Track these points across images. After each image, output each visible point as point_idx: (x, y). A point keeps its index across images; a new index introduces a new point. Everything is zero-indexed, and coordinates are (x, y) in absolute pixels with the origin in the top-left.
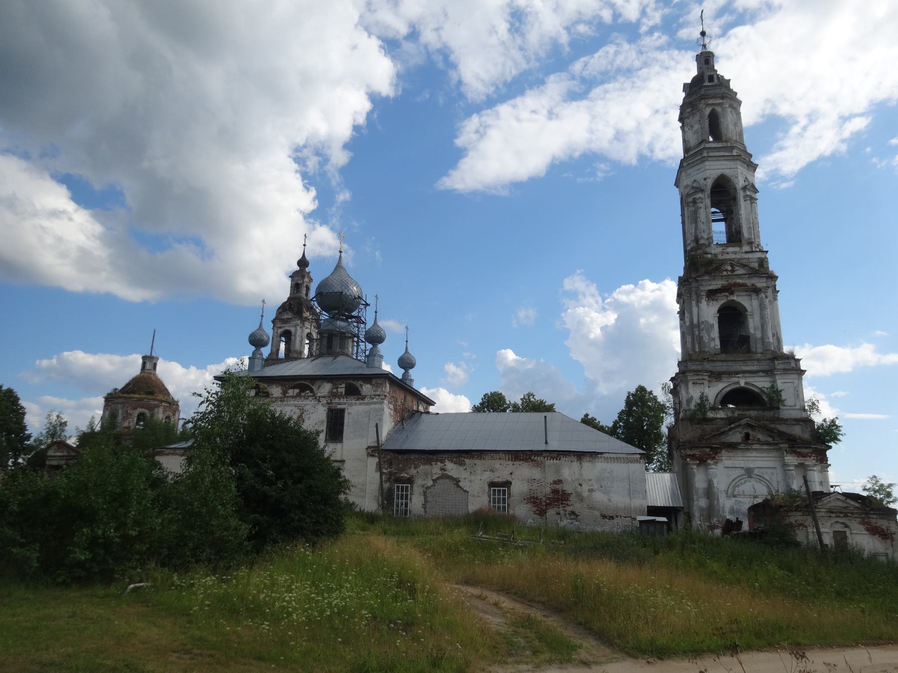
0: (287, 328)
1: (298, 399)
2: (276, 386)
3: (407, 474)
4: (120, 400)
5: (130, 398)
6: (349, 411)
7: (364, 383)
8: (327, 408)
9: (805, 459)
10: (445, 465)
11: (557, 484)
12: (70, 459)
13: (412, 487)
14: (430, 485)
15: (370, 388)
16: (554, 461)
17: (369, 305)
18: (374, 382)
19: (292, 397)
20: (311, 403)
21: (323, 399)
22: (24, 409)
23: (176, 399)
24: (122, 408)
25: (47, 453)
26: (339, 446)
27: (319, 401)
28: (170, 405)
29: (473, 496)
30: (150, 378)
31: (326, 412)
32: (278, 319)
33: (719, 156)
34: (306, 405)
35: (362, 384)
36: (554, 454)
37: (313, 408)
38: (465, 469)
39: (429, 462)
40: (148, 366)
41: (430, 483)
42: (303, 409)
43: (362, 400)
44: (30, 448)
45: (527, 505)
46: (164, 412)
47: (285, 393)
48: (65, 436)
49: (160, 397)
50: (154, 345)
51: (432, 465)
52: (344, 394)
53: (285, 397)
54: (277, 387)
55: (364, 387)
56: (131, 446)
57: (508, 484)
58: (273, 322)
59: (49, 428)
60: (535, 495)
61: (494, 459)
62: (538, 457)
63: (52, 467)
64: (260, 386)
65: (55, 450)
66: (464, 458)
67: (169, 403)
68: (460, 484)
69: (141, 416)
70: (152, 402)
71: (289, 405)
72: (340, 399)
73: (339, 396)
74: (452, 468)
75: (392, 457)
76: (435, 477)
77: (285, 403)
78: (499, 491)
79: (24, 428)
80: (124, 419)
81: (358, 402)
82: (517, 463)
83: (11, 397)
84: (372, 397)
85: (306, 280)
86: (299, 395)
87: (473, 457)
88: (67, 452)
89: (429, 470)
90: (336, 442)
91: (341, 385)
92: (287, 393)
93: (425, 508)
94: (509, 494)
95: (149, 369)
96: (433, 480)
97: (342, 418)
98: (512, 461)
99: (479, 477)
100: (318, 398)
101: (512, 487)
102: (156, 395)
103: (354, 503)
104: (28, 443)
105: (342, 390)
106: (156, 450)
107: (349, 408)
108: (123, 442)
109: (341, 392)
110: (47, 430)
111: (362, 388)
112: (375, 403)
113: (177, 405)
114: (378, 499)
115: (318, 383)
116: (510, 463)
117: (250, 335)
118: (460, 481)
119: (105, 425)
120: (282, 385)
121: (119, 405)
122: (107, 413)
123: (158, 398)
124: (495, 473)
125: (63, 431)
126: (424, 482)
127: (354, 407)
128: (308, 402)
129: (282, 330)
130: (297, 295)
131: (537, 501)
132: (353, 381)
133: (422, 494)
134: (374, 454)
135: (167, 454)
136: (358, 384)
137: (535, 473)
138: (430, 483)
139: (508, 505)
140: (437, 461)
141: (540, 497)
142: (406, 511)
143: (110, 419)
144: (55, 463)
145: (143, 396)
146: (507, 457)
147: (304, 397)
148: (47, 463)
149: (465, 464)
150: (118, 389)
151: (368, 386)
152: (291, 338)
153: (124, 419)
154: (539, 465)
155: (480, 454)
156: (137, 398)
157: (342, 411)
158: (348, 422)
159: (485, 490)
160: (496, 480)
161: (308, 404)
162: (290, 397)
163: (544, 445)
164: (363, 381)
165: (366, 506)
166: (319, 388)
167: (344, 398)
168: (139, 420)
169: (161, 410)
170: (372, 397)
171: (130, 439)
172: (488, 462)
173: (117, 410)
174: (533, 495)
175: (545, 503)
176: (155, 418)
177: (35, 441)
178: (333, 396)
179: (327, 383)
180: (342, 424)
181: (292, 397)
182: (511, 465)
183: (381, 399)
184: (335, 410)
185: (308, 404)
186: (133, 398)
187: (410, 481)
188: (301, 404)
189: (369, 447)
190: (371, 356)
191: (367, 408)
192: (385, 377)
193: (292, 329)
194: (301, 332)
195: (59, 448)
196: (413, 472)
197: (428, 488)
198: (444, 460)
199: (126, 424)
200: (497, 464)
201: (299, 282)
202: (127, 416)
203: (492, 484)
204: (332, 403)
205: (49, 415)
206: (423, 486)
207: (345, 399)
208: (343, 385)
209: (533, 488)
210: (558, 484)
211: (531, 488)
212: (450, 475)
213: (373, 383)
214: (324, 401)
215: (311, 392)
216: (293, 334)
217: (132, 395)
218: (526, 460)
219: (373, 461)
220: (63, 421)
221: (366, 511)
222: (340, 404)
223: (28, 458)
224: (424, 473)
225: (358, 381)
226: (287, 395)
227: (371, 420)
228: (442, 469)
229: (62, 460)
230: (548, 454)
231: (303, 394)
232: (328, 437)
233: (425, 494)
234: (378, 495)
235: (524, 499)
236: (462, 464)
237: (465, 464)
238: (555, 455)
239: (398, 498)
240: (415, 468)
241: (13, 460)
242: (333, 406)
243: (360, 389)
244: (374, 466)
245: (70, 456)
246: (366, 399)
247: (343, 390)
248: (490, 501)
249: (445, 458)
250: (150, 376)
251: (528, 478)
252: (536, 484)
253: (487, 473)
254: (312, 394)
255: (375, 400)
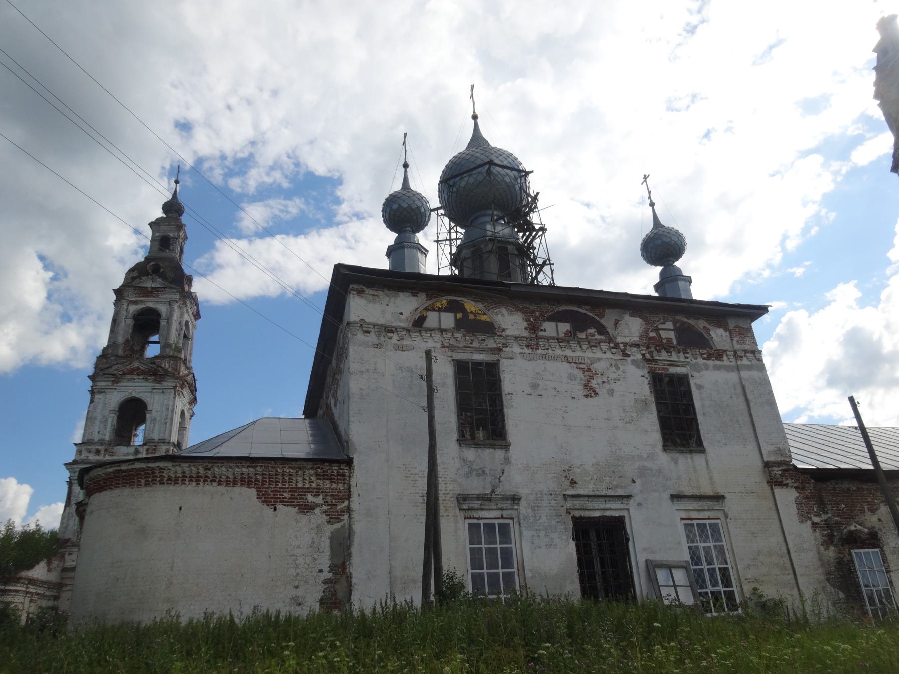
0: (151, 305)
3: (860, 525)
6: (698, 381)
9: (631, 538)
20: (604, 356)
21: (635, 349)
31: (646, 382)
32: (132, 286)
35: (708, 326)
37: (614, 369)
42: (589, 370)
43: (717, 359)
47: (533, 328)
58: (118, 292)
72: (668, 352)
73: (667, 347)
77: (540, 352)
81: (710, 363)
86: (569, 338)
91: (663, 323)
100: (621, 346)
117: (387, 200)
129: (139, 307)
151: (720, 331)
152: (159, 323)
158: (703, 406)
161: (599, 360)
185: (599, 360)
188: (583, 358)
193: (163, 309)
194: (179, 314)
215: (600, 333)
216: (164, 315)
221: (282, 617)
222: (673, 364)
226: (541, 333)
242: (659, 368)
254: (602, 337)
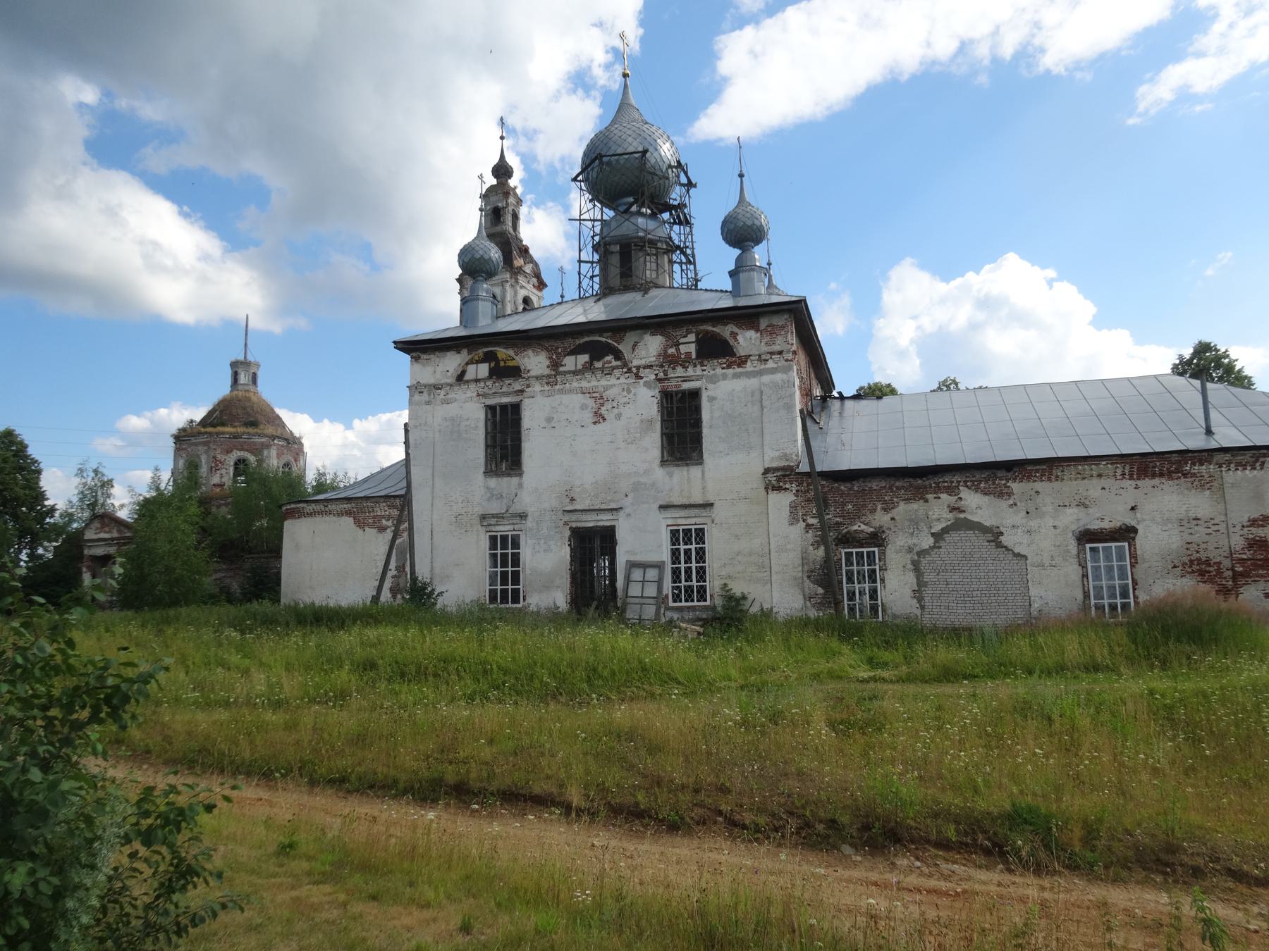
1: (588, 375)
2: (533, 351)
4: (201, 439)
5: (218, 434)
6: (710, 393)
7: (740, 327)
8: (657, 391)
10: (960, 498)
11: (1259, 526)
12: (125, 544)
13: (883, 553)
14: (927, 547)
15: (756, 339)
16: (1247, 472)
17: (695, 186)
18: (764, 323)
19: (575, 373)
20: (618, 381)
22: (39, 464)
23: (297, 435)
24: (206, 452)
25: (83, 534)
26: (695, 471)
27: (638, 377)
28: (289, 443)
29: (1041, 565)
30: (249, 399)
31: (656, 401)
33: (345, 499)
34: (606, 388)
35: (736, 330)
36: (1245, 455)
37: (625, 393)
38: (1011, 506)
39: (919, 495)
40: (243, 379)
41: (927, 542)
42: (602, 397)
43: (739, 366)
44: (57, 530)
45: (1184, 580)
46: (279, 456)
47: (555, 365)
48: (113, 504)
49: (270, 430)
50: (248, 342)
51: (926, 501)
52: (694, 356)
53: (558, 373)
54: (537, 354)
55: (740, 338)
56: (229, 516)
57: (1126, 533)
59: (82, 492)
60: (1203, 556)
61: (1084, 478)
62: (1201, 464)
63: (95, 559)
64: (500, 356)
65: (97, 529)
66: (1007, 480)
67: (286, 440)
68: (1004, 540)
69: (241, 465)
70: (257, 440)
71: (570, 391)
72: (685, 367)
73: (684, 362)
74: (977, 505)
75: (826, 489)
76: (937, 527)
77: (558, 387)
78: (860, 555)
79: (41, 496)
80: (211, 470)
81: (730, 371)
82: (1147, 483)
83: (12, 443)
84: (763, 357)
85: (511, 200)
86: (588, 367)
87: (1029, 477)
88: (119, 531)
89: (921, 512)
90: (687, 465)
91: (685, 337)
92: (562, 365)
93: (920, 600)
94: (1134, 556)
95: (244, 384)
96: (933, 534)
97: (698, 410)
98: (1131, 478)
99: (1050, 522)
101: (1139, 540)
102: (262, 427)
103: (744, 598)
104: (52, 521)
105: (689, 347)
106: (284, 508)
107: (710, 386)
108: (214, 510)
109: (688, 354)
110: (81, 496)
111: (736, 340)
112: (773, 371)
113: (301, 444)
114: (803, 583)
115: (630, 338)
116: (1127, 483)
117: (461, 250)
118: (1002, 534)
119: (180, 481)
120: (547, 349)
121: (200, 448)
122: (181, 463)
123: (265, 432)
124: (1091, 511)
125: (109, 496)
126: (911, 541)
127: (722, 384)
128: (613, 381)
130: (498, 229)
131: (1211, 569)
132: (714, 327)
133: (911, 566)
134: (781, 484)
135: (310, 515)
136: (725, 331)
137: (1200, 503)
138: (927, 542)
139: (1135, 582)
140: (938, 490)
141: (1214, 561)
142: (874, 609)
143: (188, 476)
144: (99, 551)
145: (240, 430)
146: (1119, 472)
147: (602, 369)
148: (86, 552)
149: (1010, 494)
150: (195, 422)
151: (751, 334)
153: (211, 470)
154: (1203, 484)
155: (1048, 467)
156: (231, 434)
157: (695, 395)
158: (712, 418)
159: (1068, 551)
160: (1095, 526)
162: (569, 372)
163: (1204, 436)
164: (736, 325)
165: (774, 601)
166: (633, 349)
167: (695, 366)
168: (237, 472)
169: (274, 452)
170: (763, 357)
171: (226, 505)
172: (1069, 486)
173: (198, 456)
174: (1196, 556)
175: (1230, 573)
176: (264, 465)
177: (61, 515)
178: (671, 363)
179: (653, 334)
180: (698, 423)
181: (575, 373)
182: (1131, 489)
183: (787, 360)
184: (677, 393)
186: (223, 433)
187: (877, 539)
188: (597, 387)
189: (767, 471)
190: (743, 271)
191: (753, 383)
192: (790, 311)
195: (103, 525)
196: (881, 518)
197: (922, 553)
198: (957, 487)
199: (216, 479)
200: (1093, 488)
201: (500, 205)
202: (216, 466)
203: (1086, 536)
204: (668, 379)
205: (80, 469)
206: (910, 550)
207: (699, 366)
208: (692, 337)
209: (1194, 538)
210: (1263, 526)
211: (1189, 539)
212: (976, 519)
213: (763, 325)
214: (649, 376)
217: (220, 429)
218: (1169, 475)
219: (781, 502)
220: (106, 480)
223: (55, 547)
224: (910, 520)
225: (726, 324)
226: (561, 369)
227: (765, 410)
228: (953, 509)
229: (111, 545)
230: (1228, 457)
231: (598, 364)
232: (665, 454)
233: (916, 565)
234: (800, 574)
235: (1175, 567)
236: (1004, 494)
237: (1010, 494)
238: (1248, 456)
239: (850, 580)
240: (886, 510)
241: (28, 551)
242: (672, 386)
243: (732, 342)
244: (786, 512)
245: (123, 538)
246: (749, 363)
247: (692, 349)
248: (1085, 576)
249: (959, 482)
250: (247, 395)
251: (1181, 516)
252: (1202, 530)
253: (1069, 511)
254: (619, 363)
255: (770, 364)
